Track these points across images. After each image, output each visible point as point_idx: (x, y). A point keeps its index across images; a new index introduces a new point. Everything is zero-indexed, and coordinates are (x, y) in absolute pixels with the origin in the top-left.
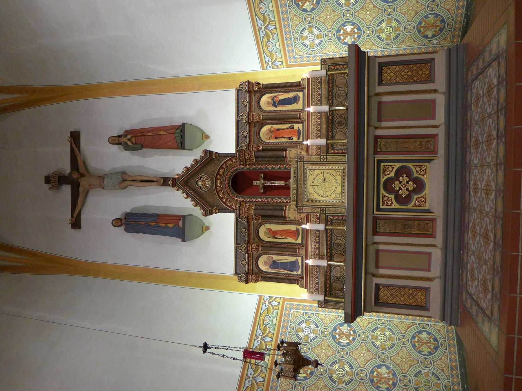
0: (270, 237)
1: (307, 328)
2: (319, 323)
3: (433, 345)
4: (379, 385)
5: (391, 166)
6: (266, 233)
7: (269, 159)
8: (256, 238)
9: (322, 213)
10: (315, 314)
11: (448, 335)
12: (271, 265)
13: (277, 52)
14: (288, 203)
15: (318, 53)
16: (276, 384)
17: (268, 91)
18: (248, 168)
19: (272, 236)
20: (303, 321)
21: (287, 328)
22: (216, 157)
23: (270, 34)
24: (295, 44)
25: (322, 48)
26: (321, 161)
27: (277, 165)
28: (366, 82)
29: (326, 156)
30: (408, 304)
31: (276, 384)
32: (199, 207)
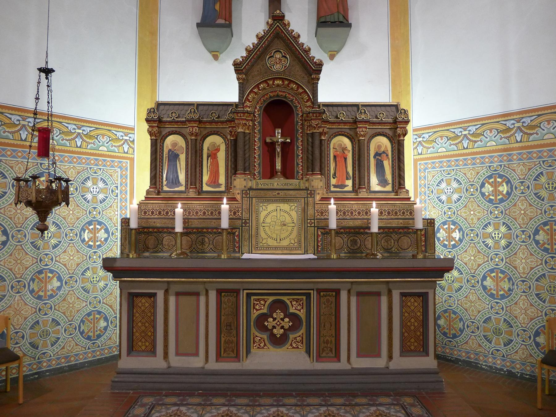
0: (208, 149)
1: (98, 190)
2: (106, 204)
3: (92, 335)
4: (37, 280)
5: (303, 308)
6: (213, 144)
7: (310, 152)
8: (206, 132)
9: (242, 221)
10: (117, 198)
11: (106, 349)
12: (173, 152)
13: (434, 148)
14: (254, 176)
15: (429, 198)
16: (19, 157)
17: (395, 146)
18: (297, 122)
19: (210, 152)
20: (107, 184)
21: (96, 165)
22: (313, 79)
23: (457, 142)
24: (442, 171)
25: (435, 203)
26: (307, 219)
27: (302, 162)
28: (406, 279)
29: (314, 227)
30: (135, 330)
31: (19, 157)
32: (245, 55)
